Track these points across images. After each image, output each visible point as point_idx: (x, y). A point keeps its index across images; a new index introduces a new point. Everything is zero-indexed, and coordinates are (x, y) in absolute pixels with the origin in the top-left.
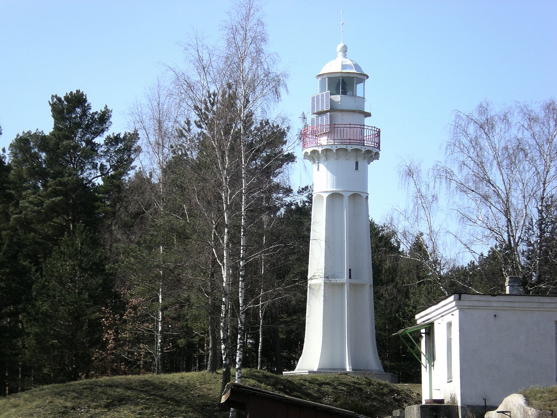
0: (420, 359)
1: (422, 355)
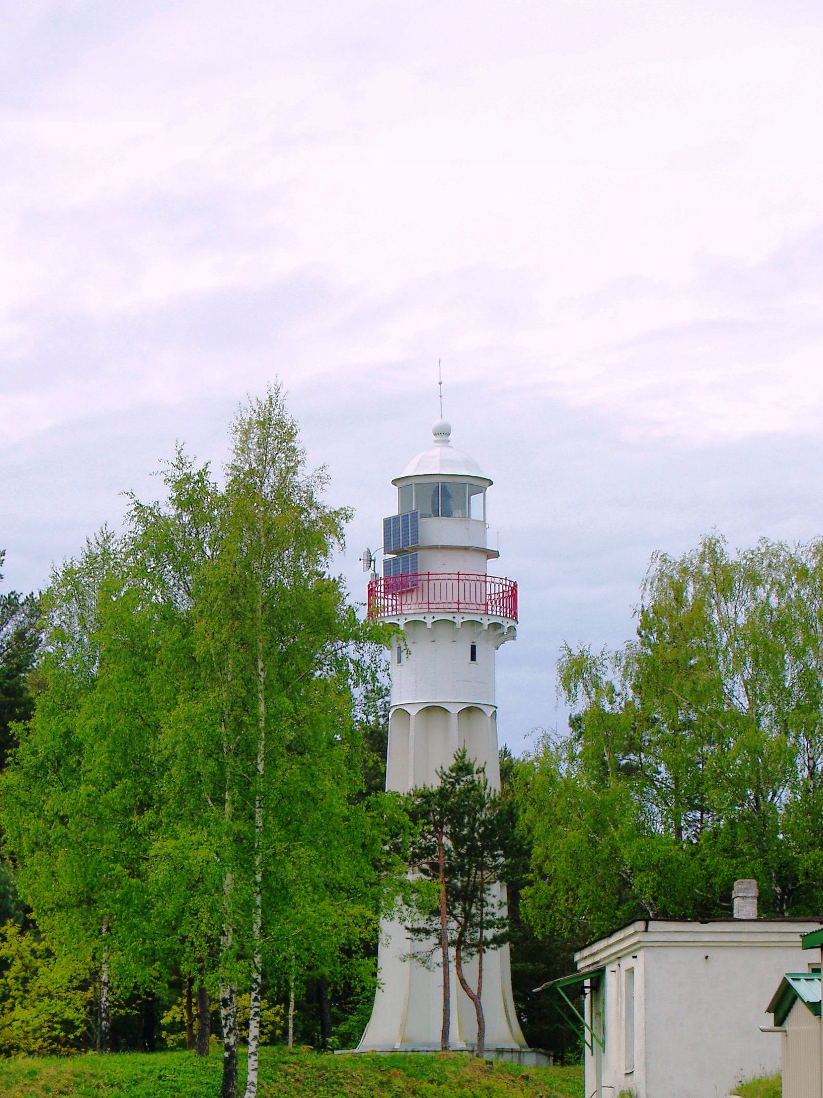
0: (583, 1033)
1: (586, 1028)
